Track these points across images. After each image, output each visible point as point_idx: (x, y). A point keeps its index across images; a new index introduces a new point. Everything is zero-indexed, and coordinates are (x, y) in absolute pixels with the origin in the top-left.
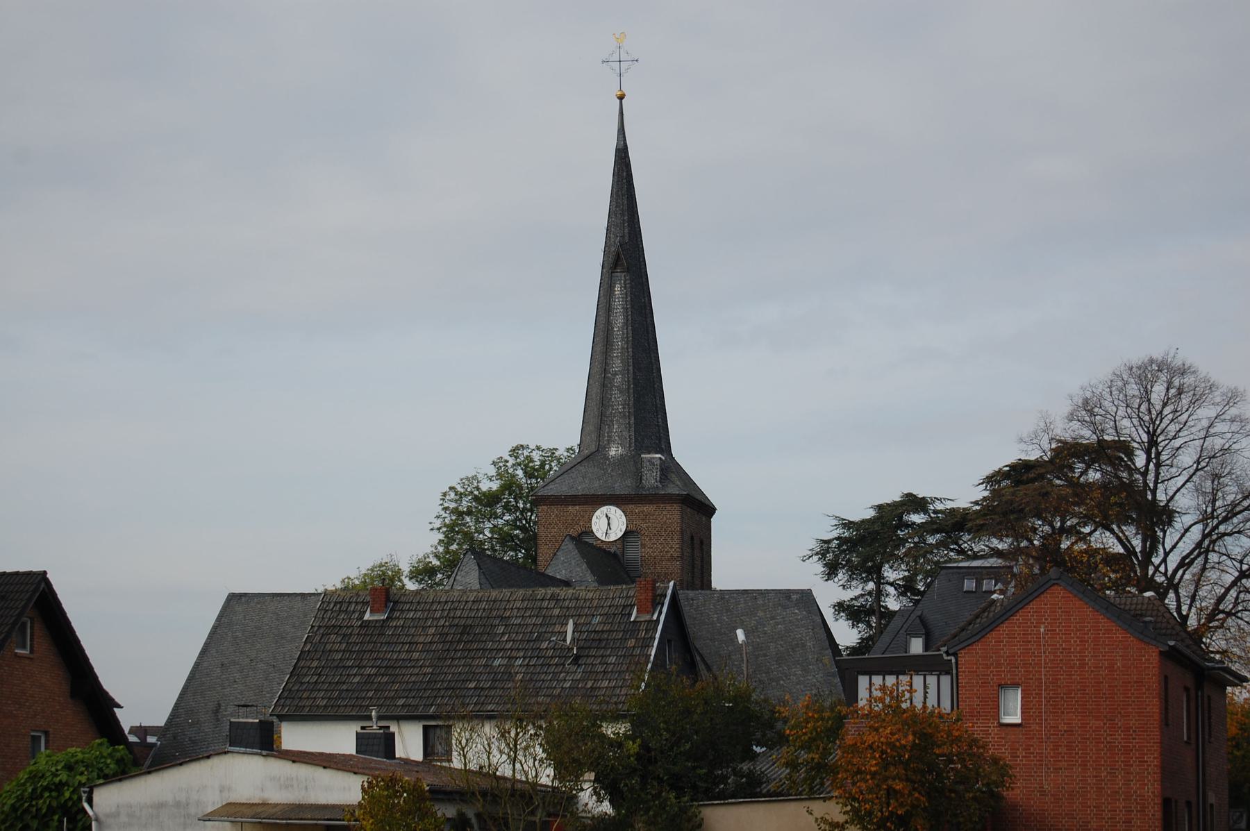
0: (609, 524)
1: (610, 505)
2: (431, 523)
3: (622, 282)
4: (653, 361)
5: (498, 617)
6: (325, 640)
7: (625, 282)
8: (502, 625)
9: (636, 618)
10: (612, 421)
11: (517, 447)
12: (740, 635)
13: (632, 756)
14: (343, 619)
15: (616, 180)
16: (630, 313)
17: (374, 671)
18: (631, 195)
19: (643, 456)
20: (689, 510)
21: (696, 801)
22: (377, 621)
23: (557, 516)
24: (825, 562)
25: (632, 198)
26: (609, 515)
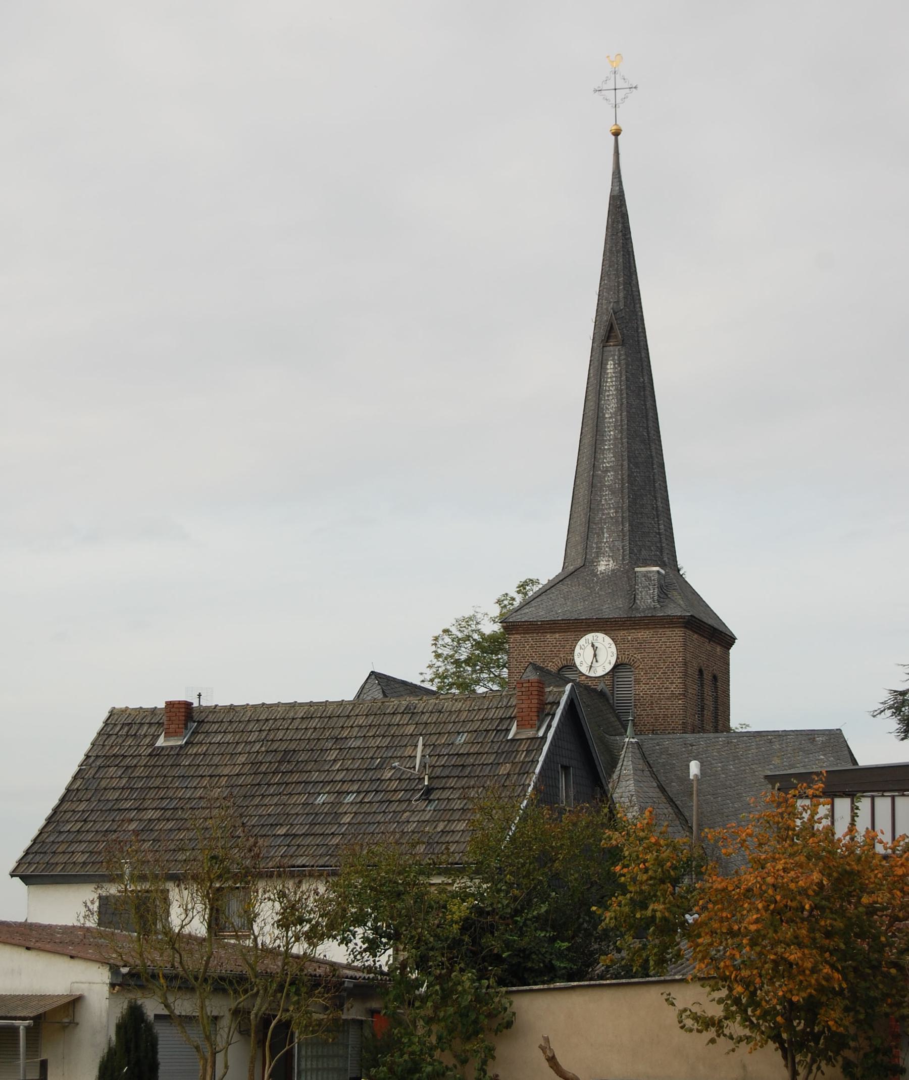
0: (595, 655)
1: (597, 631)
2: (421, 674)
3: (616, 357)
4: (654, 454)
5: (332, 738)
6: (100, 774)
7: (619, 357)
8: (336, 749)
9: (515, 734)
10: (602, 529)
11: (526, 582)
12: (694, 768)
13: (456, 923)
14: (130, 746)
15: (609, 234)
16: (625, 395)
17: (158, 814)
18: (628, 251)
19: (637, 569)
20: (696, 636)
21: (506, 985)
22: (172, 747)
23: (532, 647)
24: (899, 717)
25: (629, 255)
26: (596, 645)
